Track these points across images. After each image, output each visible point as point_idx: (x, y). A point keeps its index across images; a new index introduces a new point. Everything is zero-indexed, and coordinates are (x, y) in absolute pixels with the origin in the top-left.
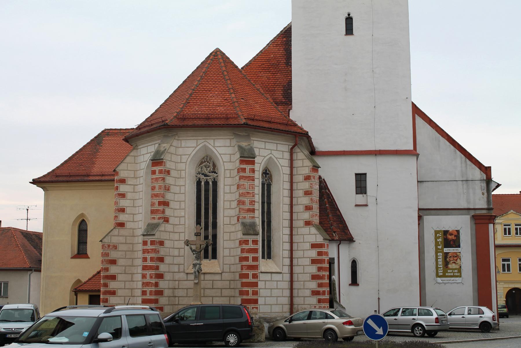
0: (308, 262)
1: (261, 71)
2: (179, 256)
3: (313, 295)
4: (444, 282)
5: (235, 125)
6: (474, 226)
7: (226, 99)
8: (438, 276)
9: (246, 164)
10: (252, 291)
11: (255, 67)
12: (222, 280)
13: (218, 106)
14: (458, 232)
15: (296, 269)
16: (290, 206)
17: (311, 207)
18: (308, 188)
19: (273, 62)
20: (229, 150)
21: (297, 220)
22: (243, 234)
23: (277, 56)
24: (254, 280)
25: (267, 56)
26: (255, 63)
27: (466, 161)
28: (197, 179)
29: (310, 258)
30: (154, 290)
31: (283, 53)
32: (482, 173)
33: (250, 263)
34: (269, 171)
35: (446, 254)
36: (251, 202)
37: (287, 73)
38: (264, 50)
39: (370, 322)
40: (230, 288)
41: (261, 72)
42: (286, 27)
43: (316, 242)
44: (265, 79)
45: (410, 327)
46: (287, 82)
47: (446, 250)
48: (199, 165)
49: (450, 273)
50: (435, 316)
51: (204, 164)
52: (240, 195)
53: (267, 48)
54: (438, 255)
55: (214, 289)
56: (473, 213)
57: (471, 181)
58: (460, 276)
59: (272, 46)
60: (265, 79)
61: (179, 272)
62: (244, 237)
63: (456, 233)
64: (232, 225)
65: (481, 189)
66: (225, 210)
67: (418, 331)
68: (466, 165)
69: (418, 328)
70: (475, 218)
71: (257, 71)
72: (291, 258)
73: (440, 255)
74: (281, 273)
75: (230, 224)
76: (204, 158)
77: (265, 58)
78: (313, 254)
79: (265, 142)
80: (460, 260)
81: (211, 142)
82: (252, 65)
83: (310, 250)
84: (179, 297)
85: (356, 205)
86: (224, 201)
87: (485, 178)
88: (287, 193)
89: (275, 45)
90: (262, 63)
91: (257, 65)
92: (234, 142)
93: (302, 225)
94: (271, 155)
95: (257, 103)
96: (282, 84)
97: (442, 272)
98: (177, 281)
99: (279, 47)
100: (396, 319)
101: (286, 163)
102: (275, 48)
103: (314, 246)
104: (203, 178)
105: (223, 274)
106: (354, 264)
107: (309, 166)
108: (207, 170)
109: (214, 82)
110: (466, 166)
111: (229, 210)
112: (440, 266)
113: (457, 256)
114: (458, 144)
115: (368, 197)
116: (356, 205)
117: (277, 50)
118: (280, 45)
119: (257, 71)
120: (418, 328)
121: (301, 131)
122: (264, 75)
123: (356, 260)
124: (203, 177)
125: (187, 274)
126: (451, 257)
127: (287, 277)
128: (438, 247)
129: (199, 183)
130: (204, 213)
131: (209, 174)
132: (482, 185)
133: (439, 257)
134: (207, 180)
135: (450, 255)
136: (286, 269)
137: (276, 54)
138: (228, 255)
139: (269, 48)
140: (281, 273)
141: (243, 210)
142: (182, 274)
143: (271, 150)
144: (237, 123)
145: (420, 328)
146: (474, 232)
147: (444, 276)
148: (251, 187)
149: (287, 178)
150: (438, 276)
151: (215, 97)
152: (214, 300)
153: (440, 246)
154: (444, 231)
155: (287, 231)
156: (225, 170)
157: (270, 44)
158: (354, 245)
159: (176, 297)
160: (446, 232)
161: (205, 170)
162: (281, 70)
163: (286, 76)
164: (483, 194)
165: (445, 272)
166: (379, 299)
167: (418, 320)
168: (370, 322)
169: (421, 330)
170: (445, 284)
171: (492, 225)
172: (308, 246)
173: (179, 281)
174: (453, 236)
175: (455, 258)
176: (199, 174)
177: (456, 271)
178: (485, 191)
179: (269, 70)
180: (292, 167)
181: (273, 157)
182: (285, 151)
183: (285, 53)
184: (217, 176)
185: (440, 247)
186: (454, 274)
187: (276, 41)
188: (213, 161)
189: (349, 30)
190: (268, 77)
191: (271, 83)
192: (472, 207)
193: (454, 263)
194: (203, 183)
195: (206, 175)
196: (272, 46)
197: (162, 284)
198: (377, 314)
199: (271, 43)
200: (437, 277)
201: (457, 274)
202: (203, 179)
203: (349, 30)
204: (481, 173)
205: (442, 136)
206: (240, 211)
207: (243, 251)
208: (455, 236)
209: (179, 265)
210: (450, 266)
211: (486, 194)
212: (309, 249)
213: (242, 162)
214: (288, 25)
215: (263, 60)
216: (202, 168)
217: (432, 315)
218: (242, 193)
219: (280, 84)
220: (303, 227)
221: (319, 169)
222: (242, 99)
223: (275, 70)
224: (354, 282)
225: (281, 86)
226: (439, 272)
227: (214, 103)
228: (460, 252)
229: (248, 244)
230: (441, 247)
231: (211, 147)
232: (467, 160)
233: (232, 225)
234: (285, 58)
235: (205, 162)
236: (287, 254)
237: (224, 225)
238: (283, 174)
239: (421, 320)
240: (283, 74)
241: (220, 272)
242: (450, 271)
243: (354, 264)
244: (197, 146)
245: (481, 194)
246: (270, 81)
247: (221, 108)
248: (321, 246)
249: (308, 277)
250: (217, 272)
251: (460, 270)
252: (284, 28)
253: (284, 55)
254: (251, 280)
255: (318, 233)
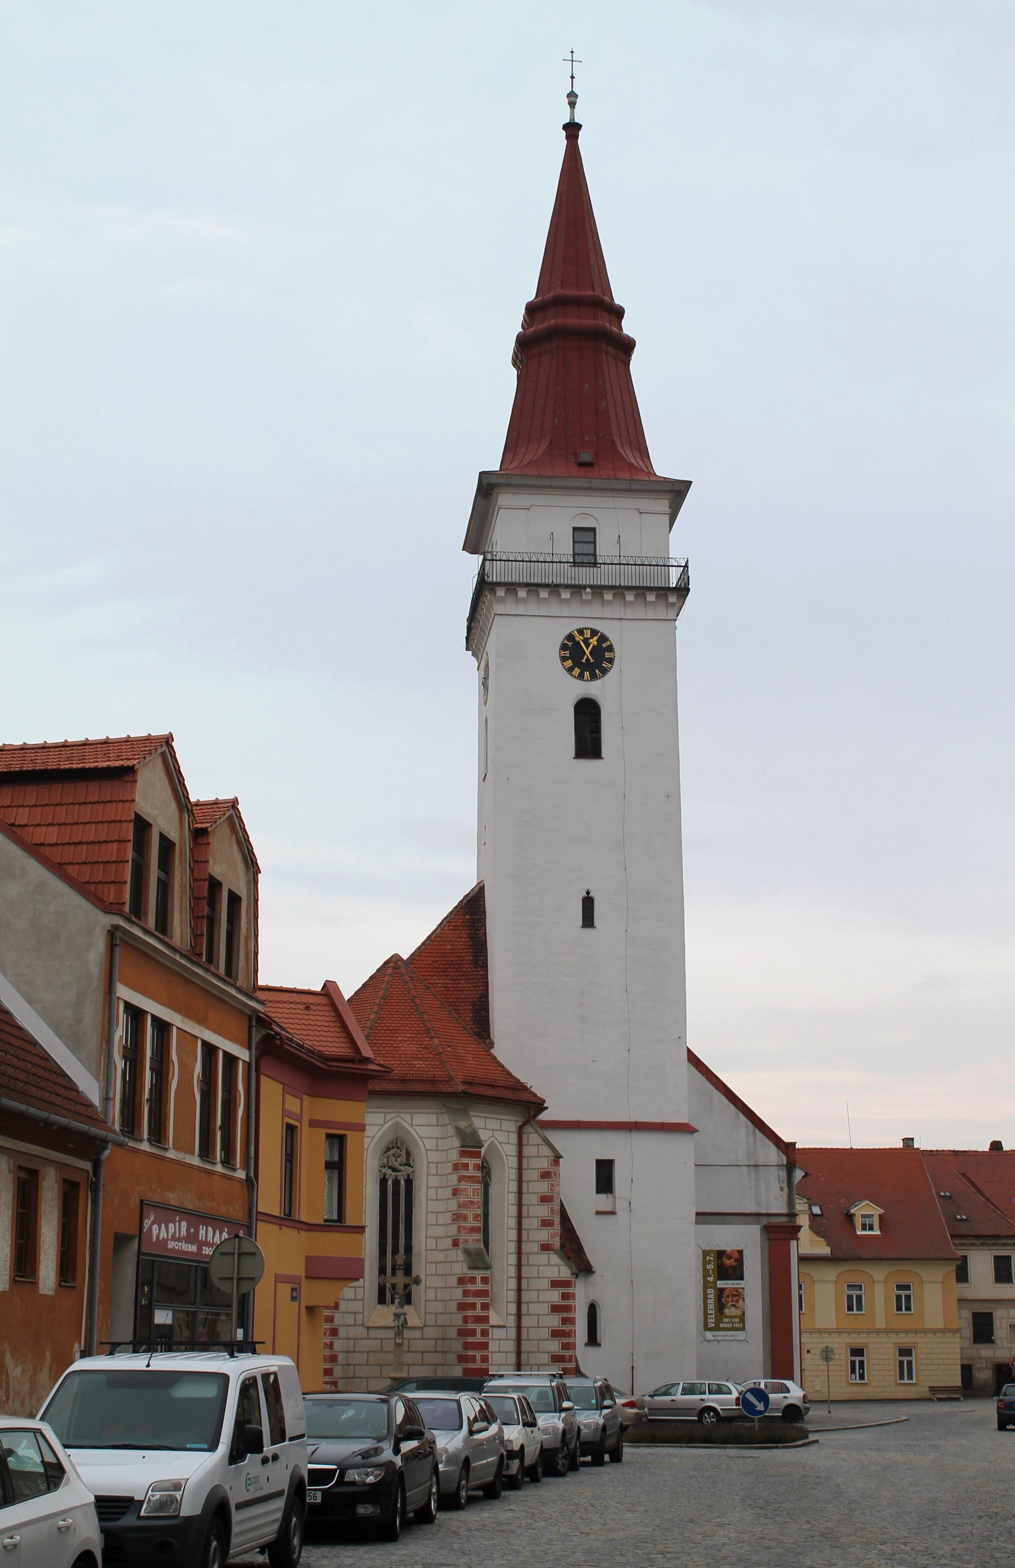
0: (546, 1309)
1: (432, 973)
2: (355, 1300)
3: (554, 1362)
4: (718, 1338)
5: (448, 1093)
6: (767, 1243)
7: (425, 1048)
8: (706, 1328)
9: (470, 1157)
10: (481, 1356)
11: (422, 966)
12: (370, 1337)
13: (416, 1059)
14: (741, 1252)
15: (526, 1321)
16: (517, 1219)
17: (552, 1221)
18: (547, 1191)
19: (452, 959)
20: (436, 1132)
21: (528, 1241)
22: (470, 1268)
23: (458, 947)
24: (483, 1340)
25: (440, 947)
26: (421, 958)
27: (754, 1133)
28: (381, 1175)
29: (548, 1303)
30: (328, 1354)
31: (467, 943)
32: (780, 1153)
33: (478, 1313)
34: (487, 1163)
35: (720, 1292)
36: (476, 1217)
37: (476, 981)
38: (434, 935)
39: (750, 1397)
40: (436, 1352)
41: (432, 976)
42: (469, 894)
43: (559, 1277)
44: (440, 989)
45: (697, 1412)
46: (478, 996)
47: (720, 1284)
48: (384, 1153)
49: (727, 1323)
50: (735, 1394)
51: (392, 1151)
52: (460, 1206)
53: (439, 931)
54: (708, 1292)
55: (411, 1352)
56: (764, 1221)
57: (762, 1167)
58: (743, 1329)
59: (447, 928)
60: (440, 989)
61: (355, 1325)
62: (470, 1272)
63: (737, 1255)
64: (439, 1250)
65: (779, 1180)
66: (429, 1227)
67: (709, 1418)
68: (755, 1138)
69: (709, 1414)
70: (768, 1229)
71: (426, 974)
72: (519, 1303)
73: (711, 1291)
74: (504, 1327)
75: (436, 1250)
76: (392, 1142)
77: (437, 951)
78: (555, 1296)
79: (486, 1118)
80: (744, 1301)
81: (407, 1117)
82: (415, 962)
83: (549, 1290)
84: (354, 1365)
85: (598, 1213)
86: (427, 1212)
87: (785, 1162)
88: (513, 1198)
89: (451, 928)
90: (432, 959)
91: (425, 962)
92: (446, 1119)
93: (536, 1250)
94: (493, 1139)
95: (467, 1052)
96: (470, 1000)
97: (714, 1321)
98: (352, 1339)
99: (458, 932)
100: (673, 1401)
101: (511, 1150)
102: (453, 932)
103: (555, 1284)
104: (391, 1175)
105: (426, 1329)
106: (592, 1310)
107: (548, 1157)
108: (396, 1161)
109: (401, 1016)
110: (755, 1142)
111: (434, 1227)
112: (711, 1312)
113: (738, 1295)
114: (743, 1103)
115: (617, 1200)
116: (598, 1213)
117: (456, 936)
118: (461, 928)
119: (426, 974)
120: (709, 1414)
121: (532, 1099)
122: (437, 981)
123: (596, 1304)
124: (390, 1171)
125: (368, 1328)
126: (729, 1296)
127: (512, 1333)
128: (708, 1279)
129: (383, 1182)
130: (405, 1231)
131: (401, 1167)
132: (781, 1173)
133: (708, 1296)
134: (396, 1177)
135: (727, 1293)
136: (512, 1321)
137: (456, 943)
138: (434, 1298)
139: (443, 931)
140: (504, 1327)
141: (465, 1229)
142: (360, 1327)
143: (493, 1130)
144: (450, 1090)
145: (712, 1414)
146: (767, 1254)
147: (717, 1328)
148: (475, 1194)
149: (513, 1174)
150: (706, 1328)
151: (407, 1042)
152: (410, 1370)
153: (710, 1276)
154: (718, 1251)
155: (513, 1259)
156: (428, 1163)
157: (443, 924)
158: (593, 1278)
159: (349, 1365)
160: (721, 1254)
161: (394, 1162)
162: (467, 973)
163: (475, 985)
164: (782, 1189)
165: (718, 1322)
166: (633, 1368)
167: (709, 1400)
168: (750, 1397)
169: (713, 1417)
170: (718, 1341)
171: (796, 1241)
172: (545, 1283)
173: (355, 1339)
174: (733, 1260)
175: (736, 1298)
176: (385, 1167)
177: (737, 1320)
178: (785, 1185)
179: (447, 973)
180: (520, 1156)
181: (495, 1141)
182: (512, 1130)
183: (471, 943)
184: (413, 1172)
185: (711, 1279)
186: (733, 1325)
187: (454, 920)
188: (406, 1148)
189: (588, 920)
190: (445, 985)
191: (451, 996)
192: (764, 1212)
193: (734, 1306)
194: (390, 1182)
195: (395, 1170)
196: (447, 928)
197: (338, 1345)
198: (757, 1386)
199: (445, 923)
200: (705, 1330)
201: (738, 1325)
202: (390, 1174)
203: (588, 920)
204: (778, 1154)
205: (717, 1088)
206: (459, 1231)
207: (466, 1293)
208: (736, 1260)
209: (355, 1313)
210: (727, 1311)
211: (786, 1189)
212: (547, 1288)
213: (463, 1154)
214: (472, 890)
215: (434, 955)
216: (388, 1158)
217: (731, 1394)
218: (463, 1203)
219: (466, 1000)
220: (538, 1253)
221: (561, 1160)
222: (448, 1046)
223: (456, 974)
224: (593, 1340)
225: (468, 1004)
226: (709, 1321)
227: (408, 1052)
228: (743, 1288)
229: (475, 1284)
230: (712, 1278)
231: (406, 1125)
232: (757, 1131)
233: (439, 1250)
234: (471, 952)
235: (393, 1148)
236: (512, 1296)
237: (427, 1250)
238: (509, 1168)
239: (713, 1400)
240: (470, 981)
241: (421, 1326)
242: (727, 1320)
243: (592, 1310)
244: (385, 1123)
245: (779, 1189)
246: (450, 993)
247: (420, 1062)
248: (567, 1284)
249: (545, 1333)
250: (416, 1325)
251: (742, 1318)
252: (466, 896)
253: (468, 947)
254: (479, 1339)
255: (563, 1264)
